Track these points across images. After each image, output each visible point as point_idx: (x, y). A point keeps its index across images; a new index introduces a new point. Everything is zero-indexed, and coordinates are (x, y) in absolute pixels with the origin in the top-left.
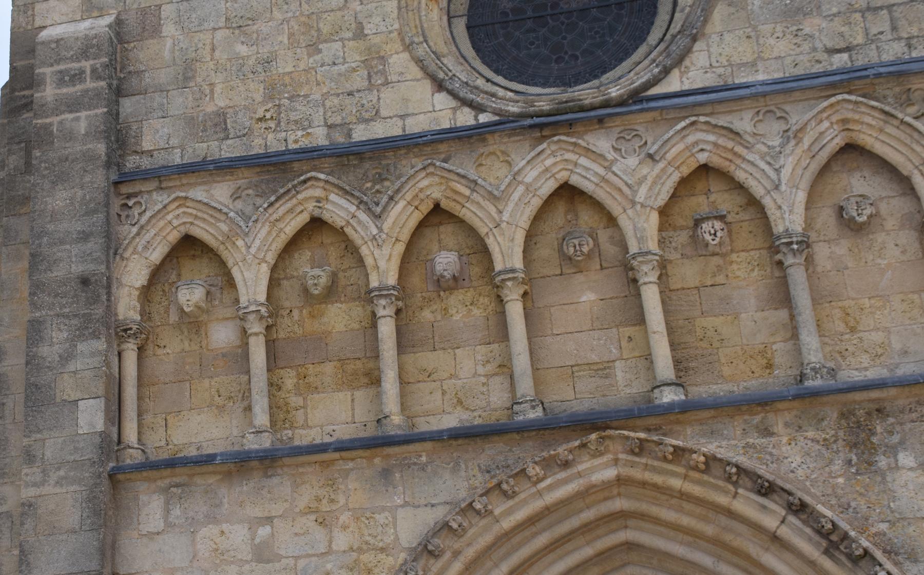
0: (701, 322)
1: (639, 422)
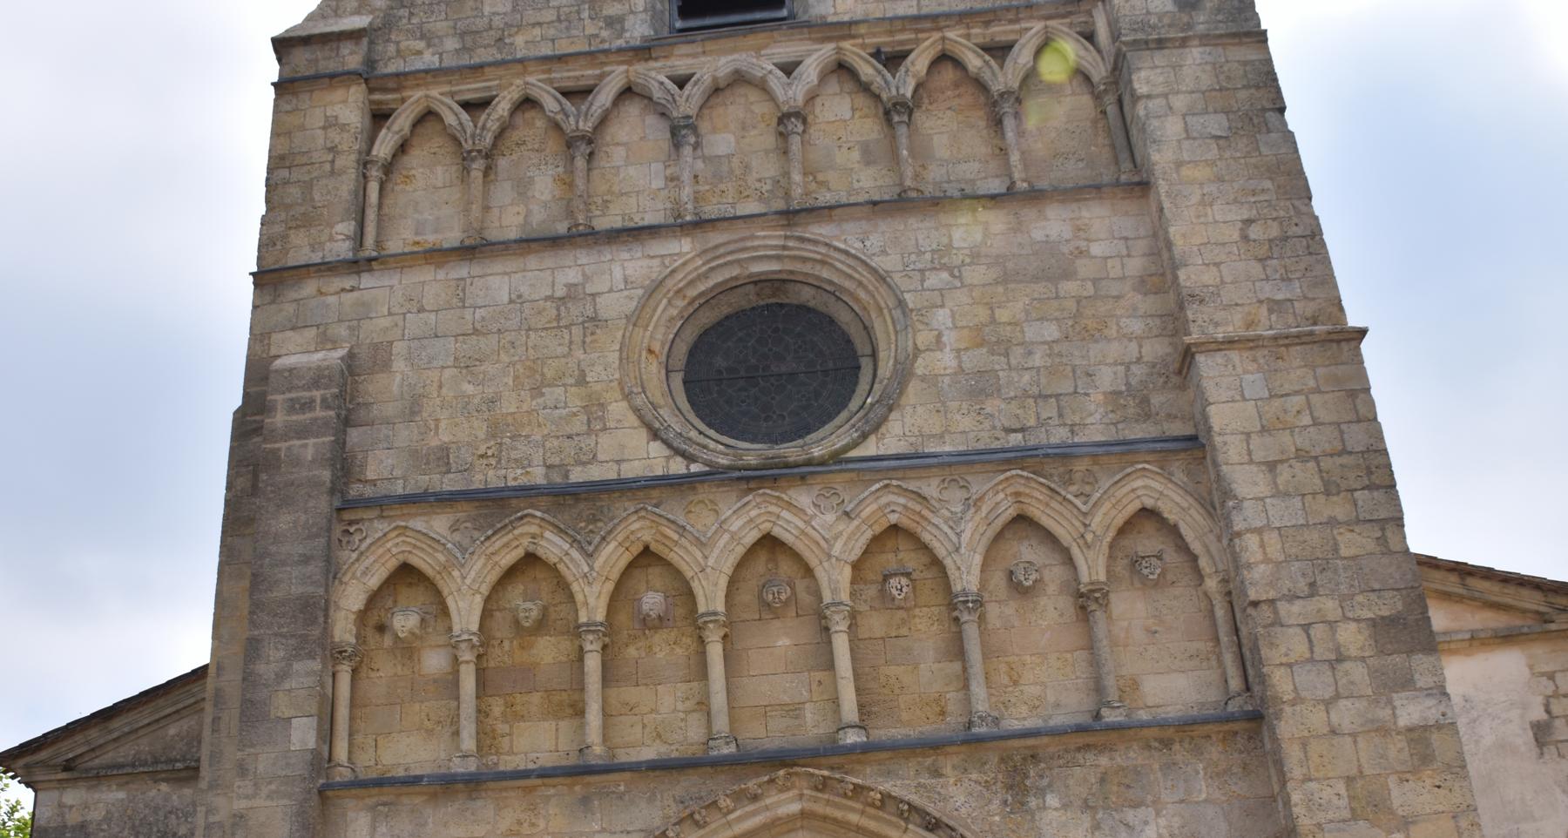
1: (823, 761)
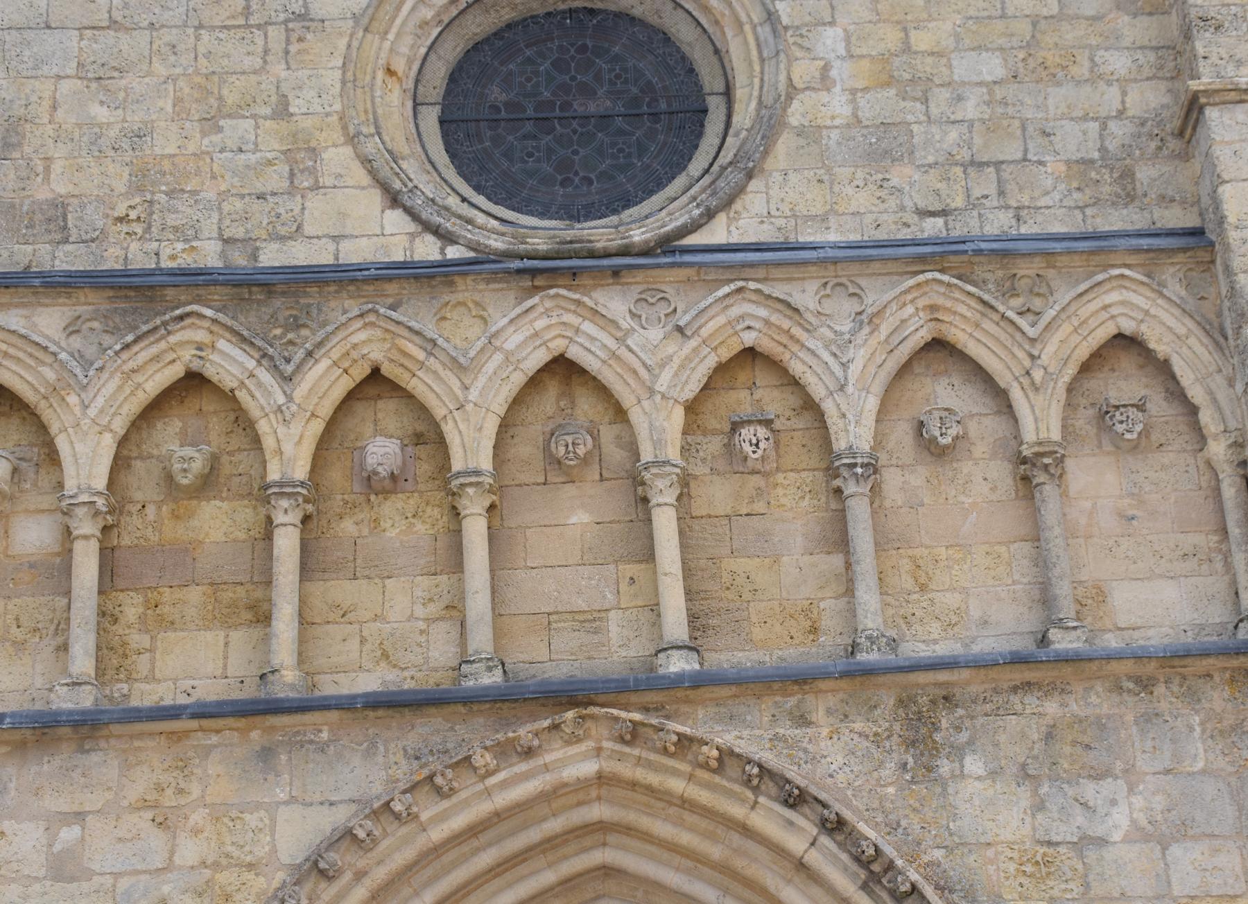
0: (730, 564)
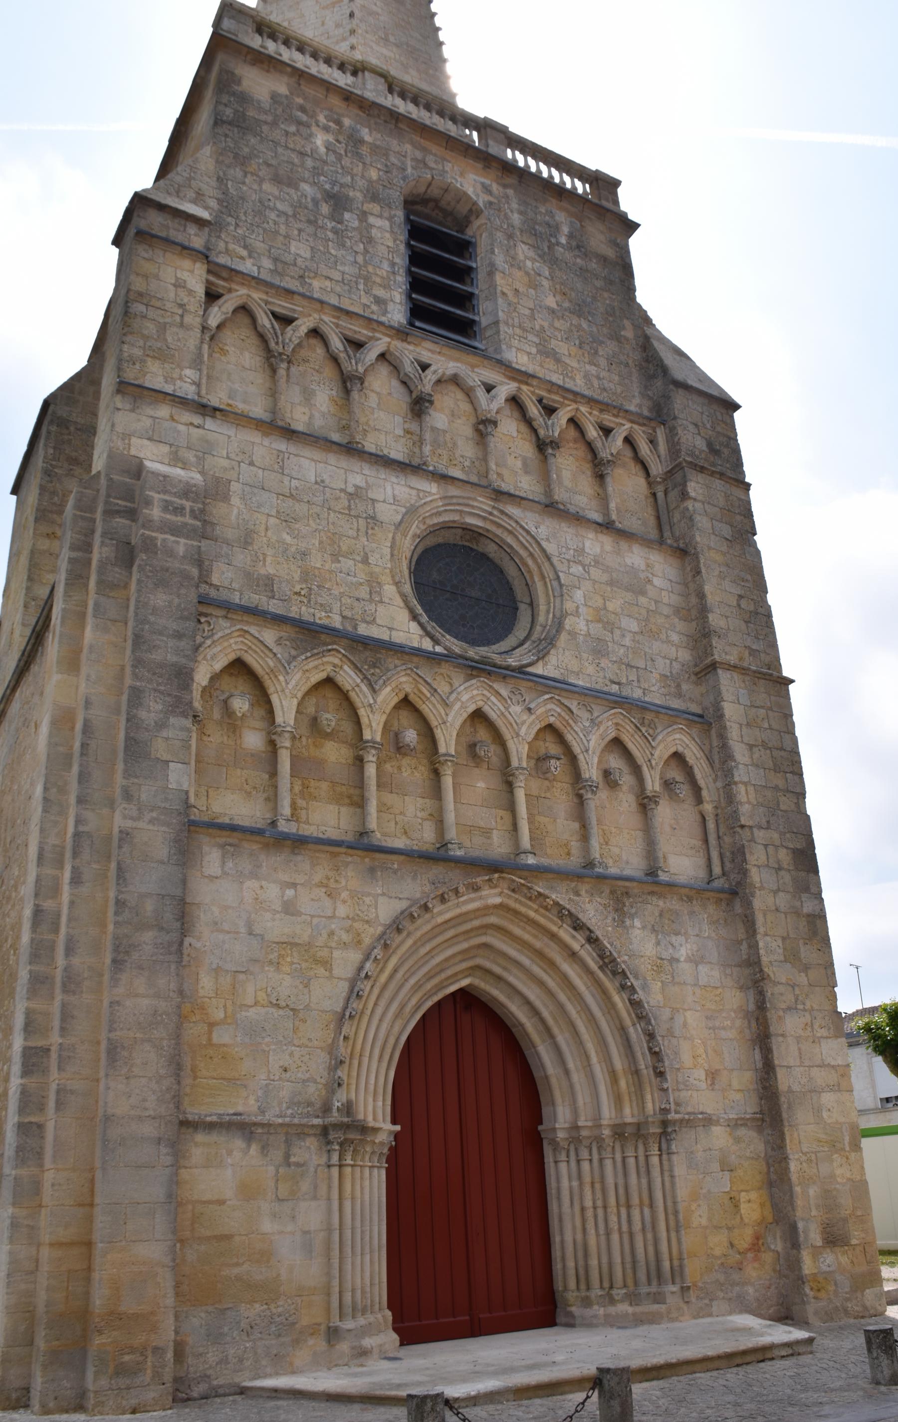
1: (518, 872)
